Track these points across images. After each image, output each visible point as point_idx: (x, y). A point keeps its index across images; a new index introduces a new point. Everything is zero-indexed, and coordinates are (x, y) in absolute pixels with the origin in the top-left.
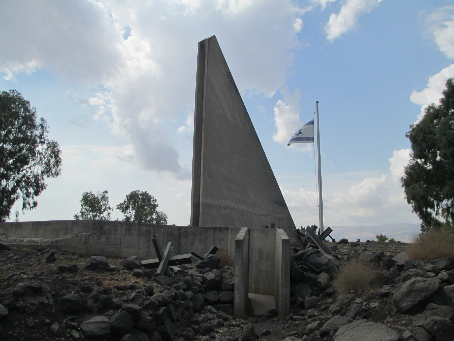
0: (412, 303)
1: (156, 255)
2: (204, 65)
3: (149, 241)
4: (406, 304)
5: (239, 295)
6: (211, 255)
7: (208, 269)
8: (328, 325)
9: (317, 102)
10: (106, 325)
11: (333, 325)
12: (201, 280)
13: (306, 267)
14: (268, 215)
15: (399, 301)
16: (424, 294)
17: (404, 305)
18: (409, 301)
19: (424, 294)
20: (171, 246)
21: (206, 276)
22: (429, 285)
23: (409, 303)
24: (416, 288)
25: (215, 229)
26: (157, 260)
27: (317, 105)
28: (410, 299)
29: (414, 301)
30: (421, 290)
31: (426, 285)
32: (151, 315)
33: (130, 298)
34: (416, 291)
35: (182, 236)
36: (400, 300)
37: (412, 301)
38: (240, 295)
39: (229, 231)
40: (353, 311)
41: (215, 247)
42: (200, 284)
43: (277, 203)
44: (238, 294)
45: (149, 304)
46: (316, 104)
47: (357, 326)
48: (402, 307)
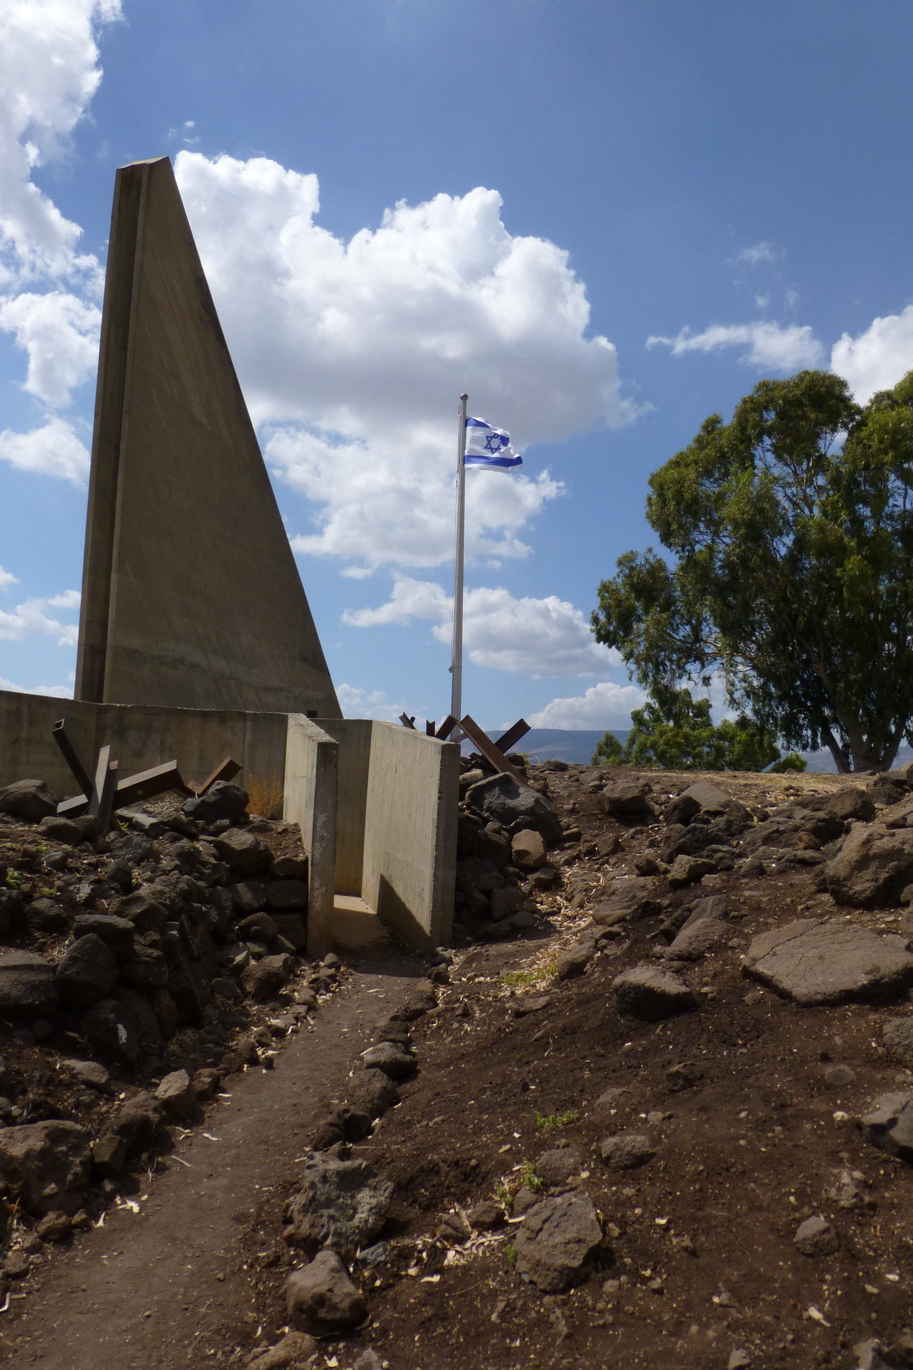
0: (874, 883)
1: (77, 785)
2: (132, 241)
3: (16, 741)
4: (862, 885)
5: (324, 889)
6: (221, 784)
7: (226, 822)
8: (693, 939)
9: (465, 397)
10: (43, 977)
11: (704, 941)
12: (214, 851)
13: (476, 817)
14: (281, 689)
15: (845, 879)
16: (896, 863)
17: (858, 888)
18: (868, 881)
19: (896, 863)
20: (111, 758)
21: (226, 841)
22: (904, 843)
23: (868, 884)
24: (876, 851)
25: (206, 716)
26: (82, 799)
27: (465, 404)
28: (868, 874)
29: (877, 880)
30: (886, 856)
31: (897, 844)
32: (153, 944)
33: (78, 899)
34: (876, 857)
35: (108, 732)
36: (848, 878)
37: (872, 880)
38: (326, 890)
39: (248, 723)
40: (712, 911)
41: (231, 761)
42: (212, 860)
43: (305, 660)
44: (321, 885)
45: (144, 913)
46: (460, 402)
47: (801, 935)
48: (855, 893)
